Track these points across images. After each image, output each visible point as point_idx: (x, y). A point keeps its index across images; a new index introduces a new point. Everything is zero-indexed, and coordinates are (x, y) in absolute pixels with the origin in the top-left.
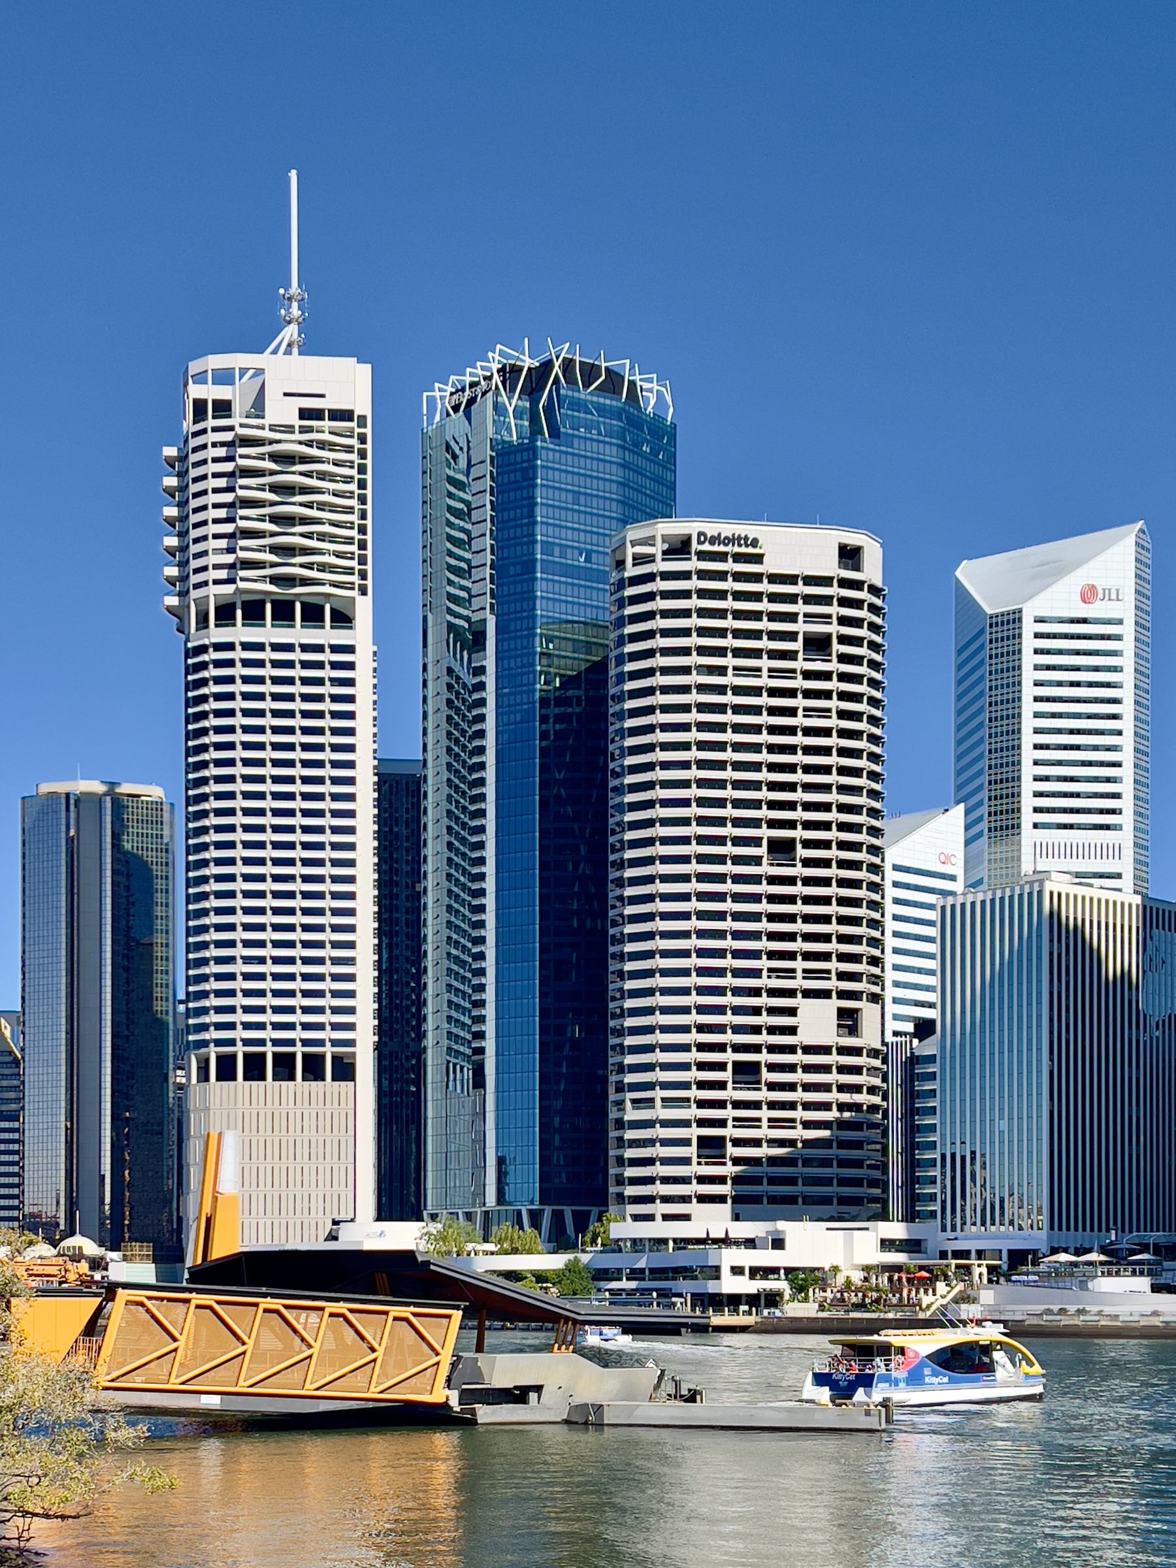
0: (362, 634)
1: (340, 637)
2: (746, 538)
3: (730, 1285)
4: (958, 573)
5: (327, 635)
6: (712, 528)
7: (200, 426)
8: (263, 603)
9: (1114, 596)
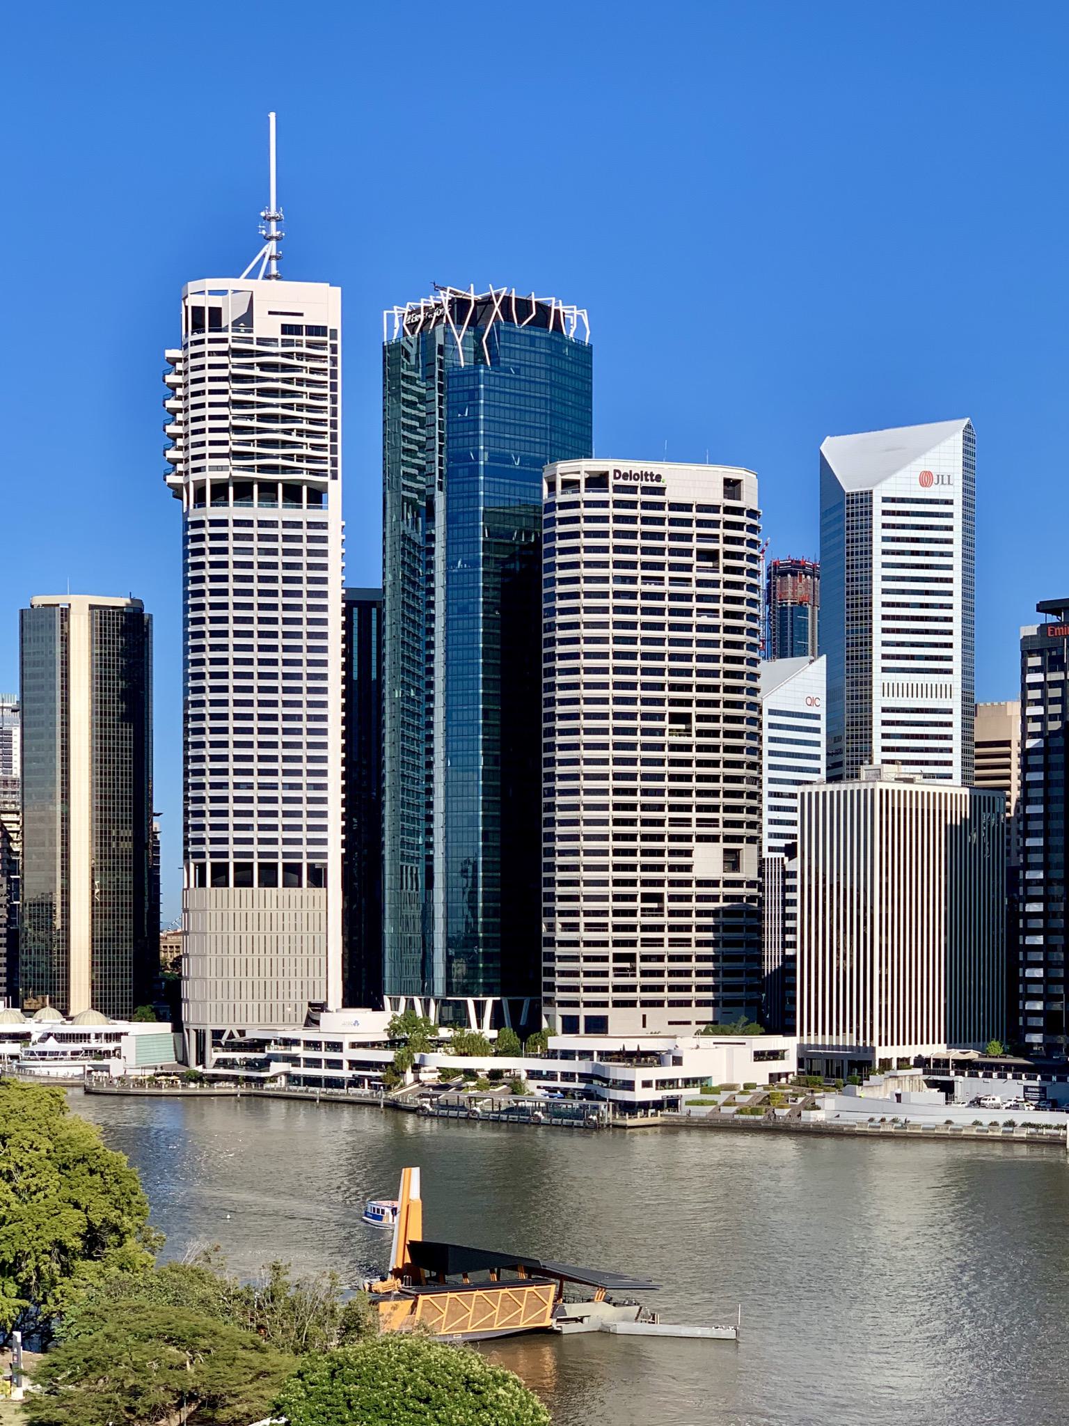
0: (333, 511)
1: (315, 515)
2: (652, 475)
3: (641, 1095)
4: (822, 448)
5: (304, 514)
6: (626, 466)
7: (198, 337)
8: (251, 484)
9: (946, 481)
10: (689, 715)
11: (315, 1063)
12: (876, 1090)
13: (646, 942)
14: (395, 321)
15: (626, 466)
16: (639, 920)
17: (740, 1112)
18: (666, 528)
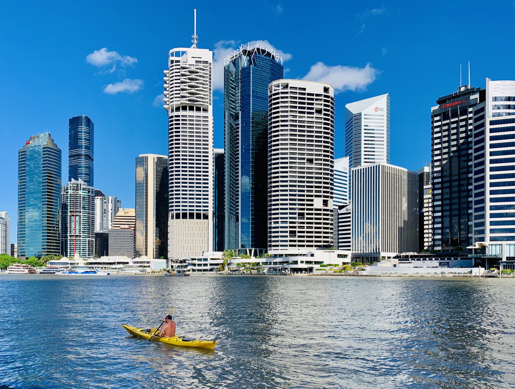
3: (300, 266)
5: (202, 114)
10: (304, 213)
11: (200, 265)
12: (382, 264)
17: (334, 272)
18: (306, 101)
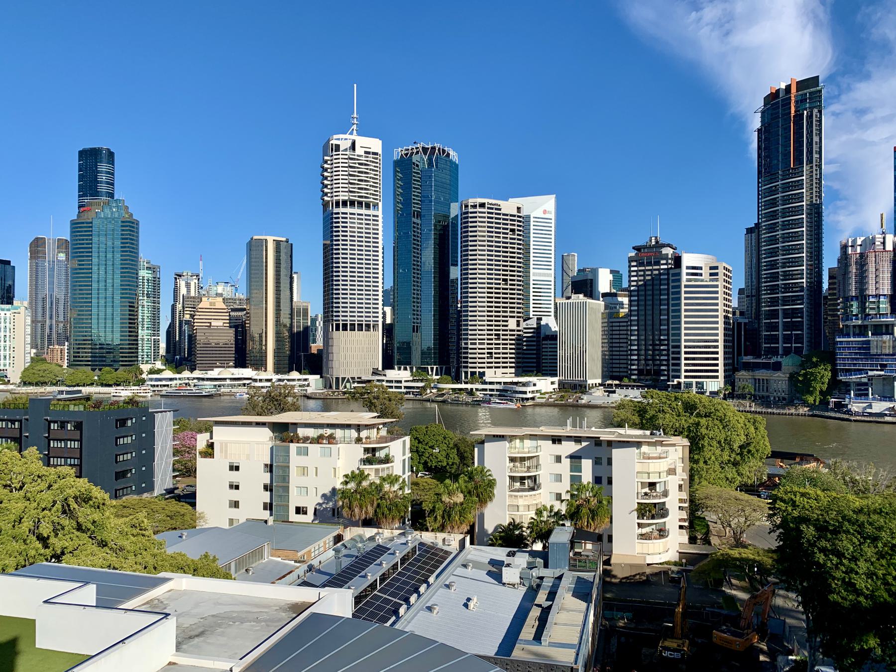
1: (375, 213)
6: (491, 201)
13: (496, 348)
14: (398, 153)
15: (491, 201)
16: (494, 341)
